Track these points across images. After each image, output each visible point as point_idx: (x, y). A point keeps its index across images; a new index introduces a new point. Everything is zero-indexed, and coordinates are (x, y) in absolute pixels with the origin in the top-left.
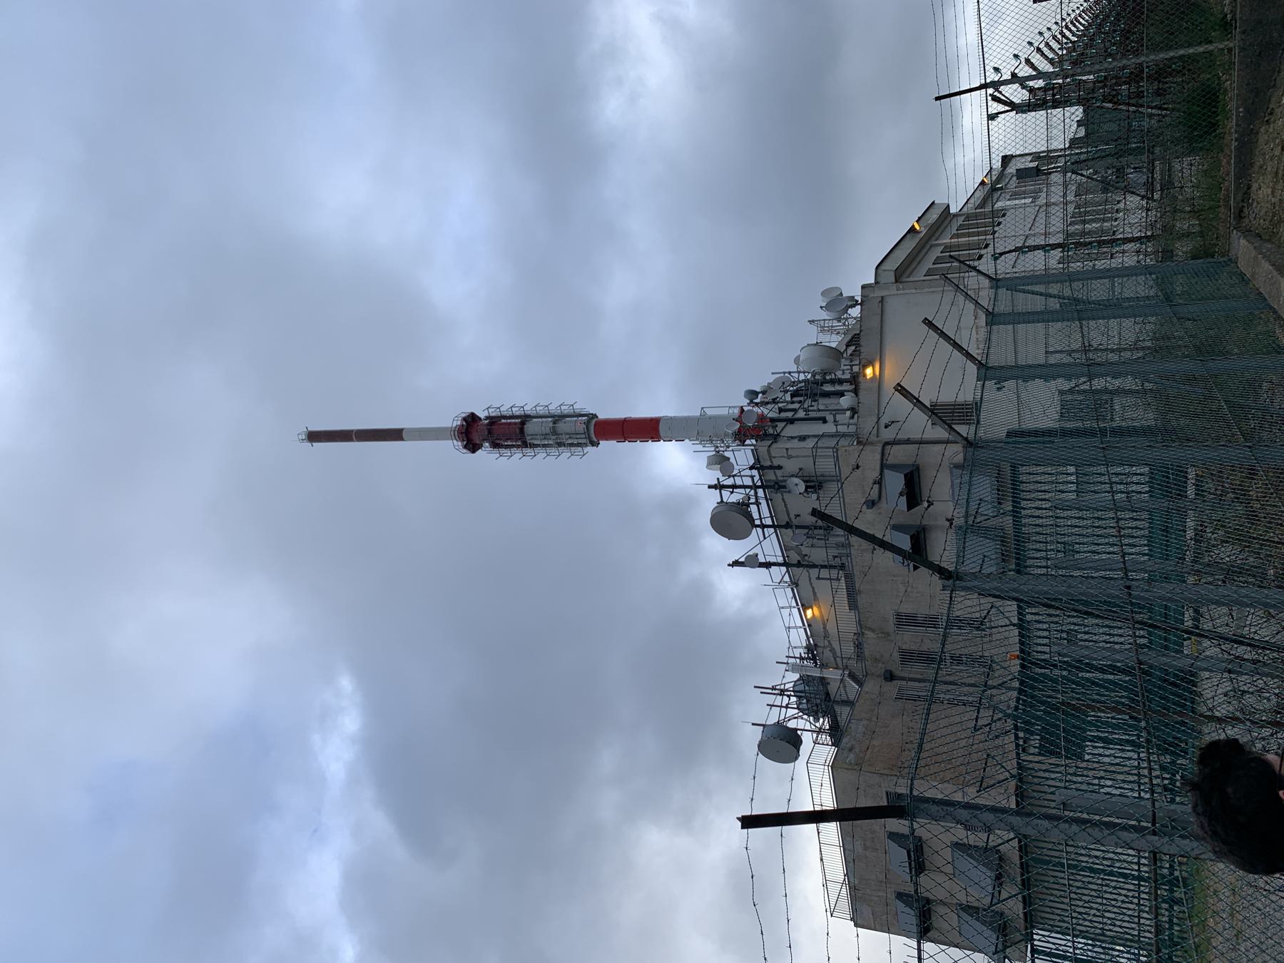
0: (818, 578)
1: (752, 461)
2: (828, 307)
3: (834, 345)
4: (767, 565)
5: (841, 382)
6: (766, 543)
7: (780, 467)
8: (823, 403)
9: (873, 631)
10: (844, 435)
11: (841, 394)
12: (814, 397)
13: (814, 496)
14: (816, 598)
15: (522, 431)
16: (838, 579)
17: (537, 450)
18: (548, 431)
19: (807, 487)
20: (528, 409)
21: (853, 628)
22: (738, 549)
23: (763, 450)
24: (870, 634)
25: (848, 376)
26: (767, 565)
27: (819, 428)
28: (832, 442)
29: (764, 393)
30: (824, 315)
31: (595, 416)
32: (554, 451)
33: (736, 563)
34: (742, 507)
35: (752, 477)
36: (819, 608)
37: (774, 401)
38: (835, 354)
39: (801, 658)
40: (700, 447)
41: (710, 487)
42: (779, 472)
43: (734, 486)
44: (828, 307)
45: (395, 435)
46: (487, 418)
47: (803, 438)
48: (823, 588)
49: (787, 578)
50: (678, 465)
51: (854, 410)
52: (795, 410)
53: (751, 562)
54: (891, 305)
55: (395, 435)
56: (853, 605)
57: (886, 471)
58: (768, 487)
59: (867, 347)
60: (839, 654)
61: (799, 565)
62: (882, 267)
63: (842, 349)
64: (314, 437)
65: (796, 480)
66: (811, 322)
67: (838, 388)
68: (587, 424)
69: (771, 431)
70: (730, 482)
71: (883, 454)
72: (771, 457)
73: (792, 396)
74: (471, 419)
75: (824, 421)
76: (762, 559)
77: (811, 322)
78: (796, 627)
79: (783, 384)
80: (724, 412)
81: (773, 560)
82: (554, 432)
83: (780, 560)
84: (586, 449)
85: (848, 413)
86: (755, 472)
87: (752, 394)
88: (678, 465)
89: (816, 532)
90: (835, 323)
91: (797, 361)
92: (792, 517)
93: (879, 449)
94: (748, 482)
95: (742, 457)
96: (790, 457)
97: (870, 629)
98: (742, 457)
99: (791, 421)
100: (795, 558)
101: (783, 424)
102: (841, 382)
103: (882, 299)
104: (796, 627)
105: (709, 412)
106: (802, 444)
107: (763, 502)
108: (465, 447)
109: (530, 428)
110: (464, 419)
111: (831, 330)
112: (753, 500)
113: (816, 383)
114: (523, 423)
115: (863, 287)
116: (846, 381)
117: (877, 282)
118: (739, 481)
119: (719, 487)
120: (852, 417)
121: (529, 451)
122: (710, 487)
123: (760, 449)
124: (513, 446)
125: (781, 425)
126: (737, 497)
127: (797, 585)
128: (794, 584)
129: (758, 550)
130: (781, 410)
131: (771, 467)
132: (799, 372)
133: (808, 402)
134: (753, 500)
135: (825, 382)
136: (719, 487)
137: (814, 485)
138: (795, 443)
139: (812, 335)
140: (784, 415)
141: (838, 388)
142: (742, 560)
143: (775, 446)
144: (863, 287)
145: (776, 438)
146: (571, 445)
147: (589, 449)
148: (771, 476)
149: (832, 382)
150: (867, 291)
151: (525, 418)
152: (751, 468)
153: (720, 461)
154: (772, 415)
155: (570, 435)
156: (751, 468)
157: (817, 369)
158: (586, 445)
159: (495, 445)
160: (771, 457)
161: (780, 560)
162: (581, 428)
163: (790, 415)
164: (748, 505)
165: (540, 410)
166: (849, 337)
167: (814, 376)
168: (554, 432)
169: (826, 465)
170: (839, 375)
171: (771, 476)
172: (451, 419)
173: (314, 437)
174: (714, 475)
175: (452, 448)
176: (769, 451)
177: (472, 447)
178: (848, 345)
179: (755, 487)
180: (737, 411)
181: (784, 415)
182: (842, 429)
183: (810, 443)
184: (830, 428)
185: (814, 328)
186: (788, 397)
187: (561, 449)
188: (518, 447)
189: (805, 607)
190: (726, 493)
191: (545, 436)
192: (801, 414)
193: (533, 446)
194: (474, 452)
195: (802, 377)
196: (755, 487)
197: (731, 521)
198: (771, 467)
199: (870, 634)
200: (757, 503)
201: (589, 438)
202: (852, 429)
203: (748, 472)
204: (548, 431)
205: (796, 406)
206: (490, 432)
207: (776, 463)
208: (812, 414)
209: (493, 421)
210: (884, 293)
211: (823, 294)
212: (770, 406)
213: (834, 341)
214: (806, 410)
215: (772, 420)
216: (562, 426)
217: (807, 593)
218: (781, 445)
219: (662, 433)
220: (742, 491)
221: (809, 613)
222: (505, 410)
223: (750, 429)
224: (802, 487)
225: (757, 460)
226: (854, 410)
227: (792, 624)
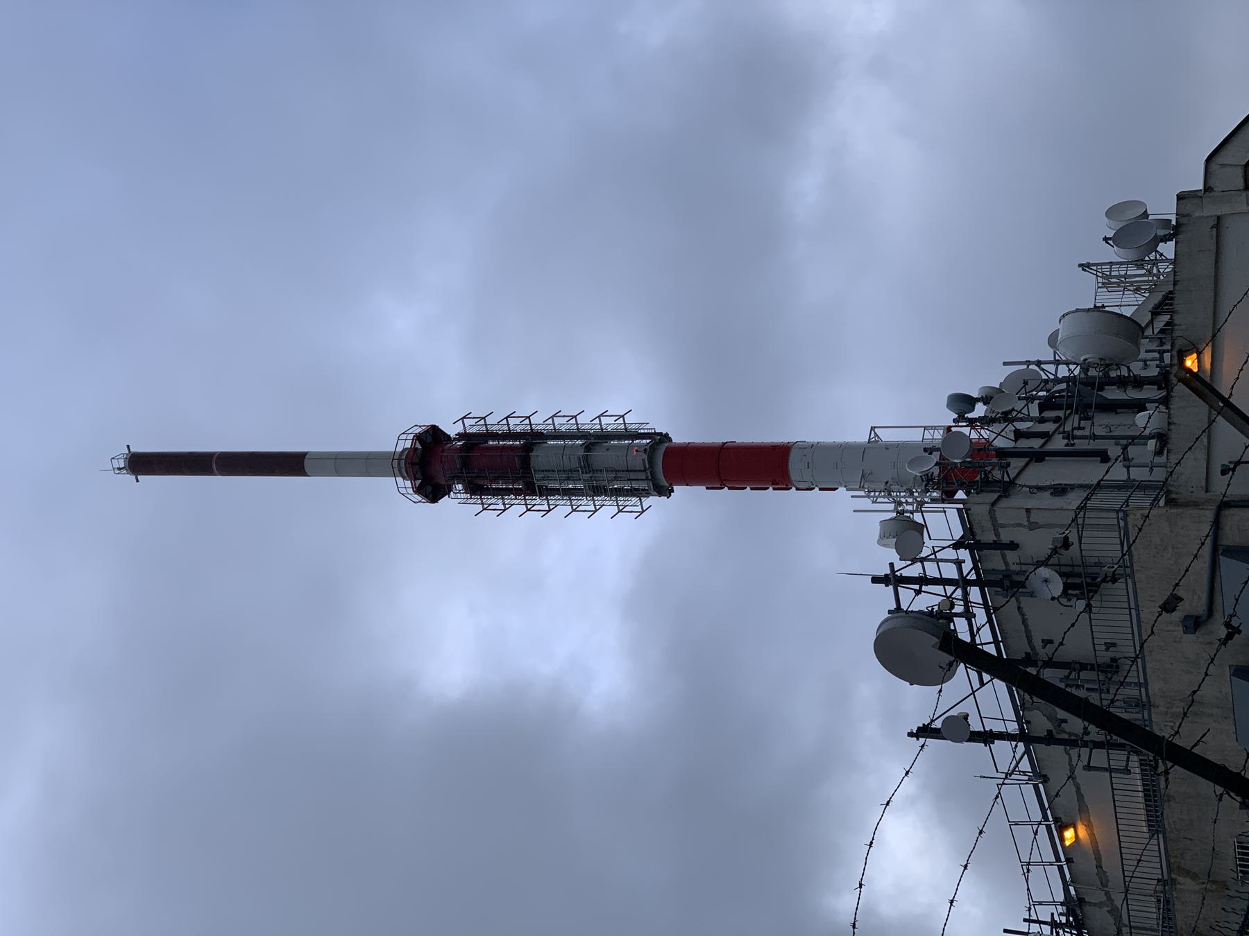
0: (1088, 767)
1: (958, 533)
2: (1114, 241)
3: (1128, 312)
4: (987, 737)
5: (1139, 382)
6: (985, 694)
7: (1013, 546)
8: (1102, 424)
9: (1194, 877)
10: (1141, 487)
11: (1139, 406)
12: (1085, 410)
13: (1081, 604)
14: (1083, 809)
15: (526, 462)
16: (1127, 771)
17: (553, 500)
18: (575, 464)
19: (1067, 587)
20: (539, 421)
21: (1153, 869)
22: (920, 703)
23: (980, 511)
24: (1185, 883)
25: (1153, 372)
26: (987, 737)
27: (1091, 472)
28: (1116, 500)
29: (986, 400)
30: (1111, 254)
31: (665, 437)
32: (585, 503)
33: (925, 732)
34: (939, 620)
35: (959, 563)
36: (1089, 826)
37: (1006, 417)
38: (1130, 328)
39: (1054, 924)
40: (866, 503)
41: (875, 580)
42: (1012, 556)
43: (923, 580)
44: (1114, 241)
45: (289, 464)
46: (461, 436)
47: (1060, 490)
48: (1096, 786)
49: (1025, 765)
50: (839, 535)
51: (1162, 439)
52: (1046, 436)
53: (953, 729)
54: (1235, 234)
55: (289, 464)
56: (1155, 823)
57: (1223, 559)
58: (990, 584)
59: (1190, 317)
60: (1125, 920)
61: (1049, 739)
62: (1220, 159)
63: (1144, 319)
64: (141, 464)
65: (1044, 572)
66: (1085, 267)
67: (1133, 394)
68: (651, 451)
69: (997, 474)
70: (915, 571)
71: (1217, 524)
72: (996, 526)
73: (1042, 408)
74: (432, 438)
75: (1104, 457)
76: (975, 726)
77: (1085, 267)
78: (1042, 863)
79: (1025, 382)
80: (915, 436)
81: (998, 727)
82: (587, 466)
83: (1013, 727)
84: (647, 502)
85: (1152, 444)
86: (964, 554)
87: (962, 403)
88: (839, 535)
89: (1083, 675)
90: (1133, 271)
91: (1053, 340)
92: (1038, 644)
93: (1209, 515)
94: (950, 572)
95: (942, 524)
96: (1033, 526)
97: (1187, 873)
98: (942, 524)
99: (1038, 457)
100: (1041, 724)
101: (1021, 462)
102: (1139, 382)
103: (1218, 223)
104: (1042, 863)
105: (886, 436)
106: (1059, 502)
107: (981, 616)
108: (418, 491)
109: (539, 458)
110: (418, 437)
111: (1124, 283)
112: (958, 609)
113: (1088, 382)
114: (528, 448)
115: (1180, 197)
116: (1150, 381)
117: (1208, 188)
118: (932, 570)
119: (893, 580)
120: (1159, 452)
121: (539, 502)
122: (875, 580)
123: (975, 510)
124: (508, 492)
125: (1016, 464)
126: (928, 600)
127: (1045, 779)
128: (1039, 776)
129: (968, 707)
130: (1019, 435)
131: (997, 545)
132: (1057, 363)
133: (1074, 420)
134: (958, 609)
135: (1106, 382)
136: (893, 580)
137: (1083, 583)
138: (1046, 500)
139: (1086, 292)
140: (1024, 444)
141: (1133, 394)
142: (938, 724)
143: (1004, 503)
144: (1180, 197)
145: (1007, 488)
146: (618, 493)
147: (652, 501)
148: (995, 561)
149: (1122, 383)
150: (1188, 207)
151: (534, 438)
152: (957, 545)
153: (905, 534)
154: (1000, 443)
155: (617, 474)
156: (957, 545)
157: (1090, 356)
158: (647, 494)
159: (476, 489)
160: (996, 526)
161: (1013, 727)
162: (638, 460)
163: (1036, 444)
164: (950, 618)
165: (562, 424)
166: (1158, 297)
167: (1085, 367)
168: (587, 466)
169: (1101, 545)
170: (1137, 369)
171: (995, 561)
172: (391, 434)
173: (141, 464)
174: (886, 558)
175: (394, 491)
176: (992, 513)
177: (432, 491)
178: (1156, 313)
179: (963, 583)
180: (939, 435)
181: (1024, 444)
182: (1138, 474)
183: (1074, 500)
184: (1118, 473)
185: (1089, 278)
186: (1034, 410)
187: (599, 500)
188: (517, 492)
189: (1062, 828)
190: (906, 594)
191: (570, 475)
192: (1059, 443)
193: (546, 493)
194: (434, 497)
195: (1063, 371)
196: (963, 583)
197: (920, 646)
198: (997, 545)
199: (1185, 883)
200: (968, 615)
201: (653, 478)
202: (1159, 474)
203: (951, 554)
204: (575, 464)
205: (1049, 427)
206: (466, 463)
207: (1005, 537)
208: (1080, 445)
209: (473, 442)
210: (1222, 210)
211: (1110, 213)
212: (997, 427)
213: (1128, 304)
214: (1069, 436)
215: (1002, 453)
216: (600, 456)
217: (1068, 797)
218: (1019, 501)
219: (794, 475)
220: (938, 589)
221: (1069, 834)
222: (494, 422)
223: (959, 471)
224: (1057, 587)
225: (969, 530)
226: (1162, 439)
227: (1036, 858)
